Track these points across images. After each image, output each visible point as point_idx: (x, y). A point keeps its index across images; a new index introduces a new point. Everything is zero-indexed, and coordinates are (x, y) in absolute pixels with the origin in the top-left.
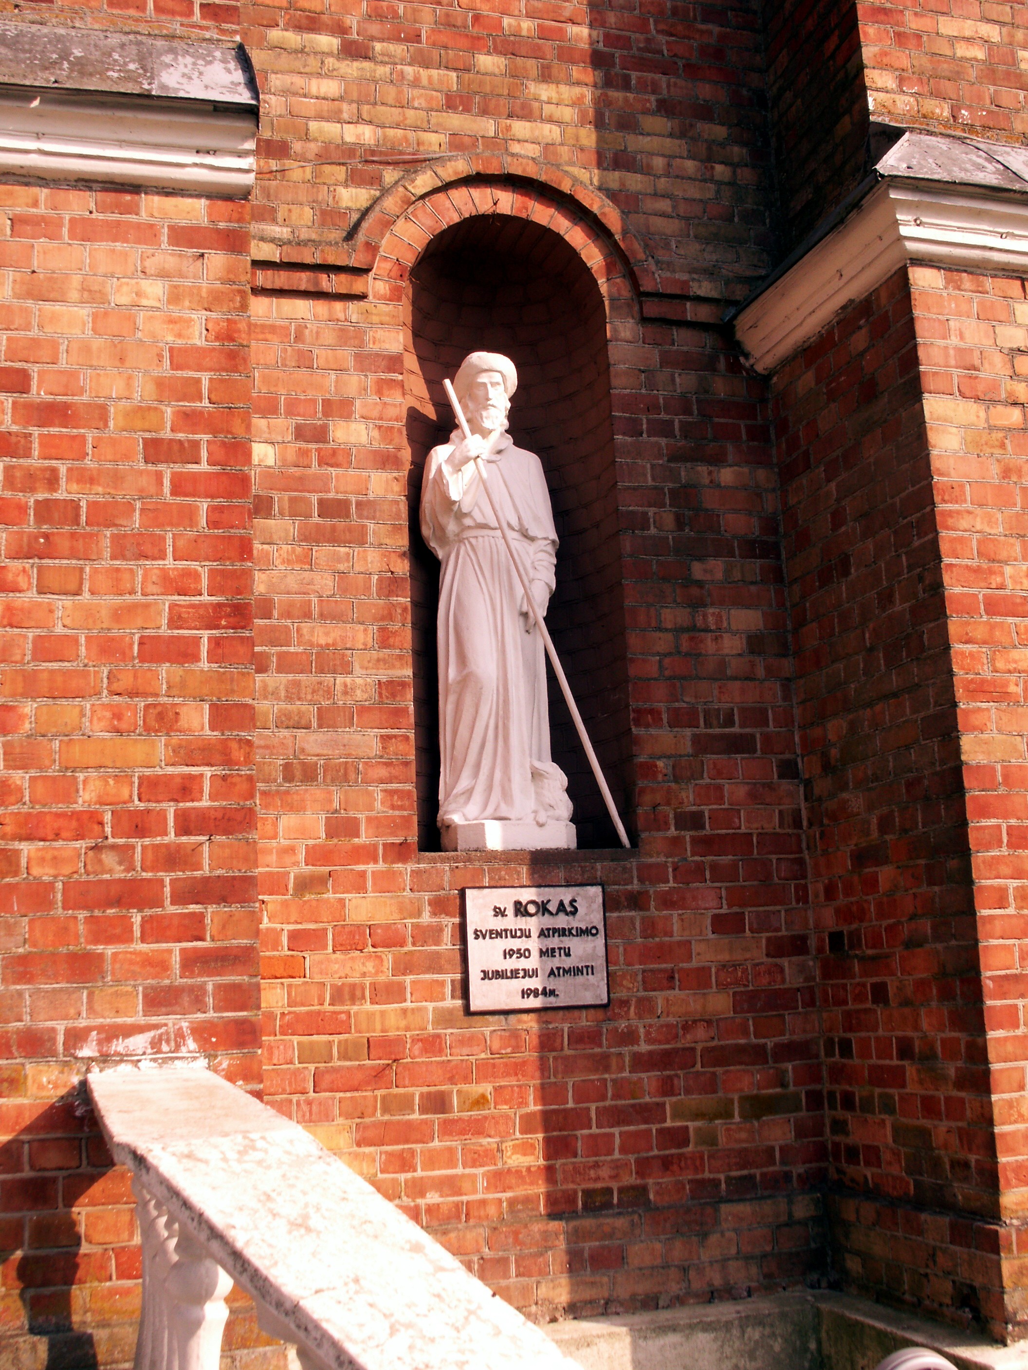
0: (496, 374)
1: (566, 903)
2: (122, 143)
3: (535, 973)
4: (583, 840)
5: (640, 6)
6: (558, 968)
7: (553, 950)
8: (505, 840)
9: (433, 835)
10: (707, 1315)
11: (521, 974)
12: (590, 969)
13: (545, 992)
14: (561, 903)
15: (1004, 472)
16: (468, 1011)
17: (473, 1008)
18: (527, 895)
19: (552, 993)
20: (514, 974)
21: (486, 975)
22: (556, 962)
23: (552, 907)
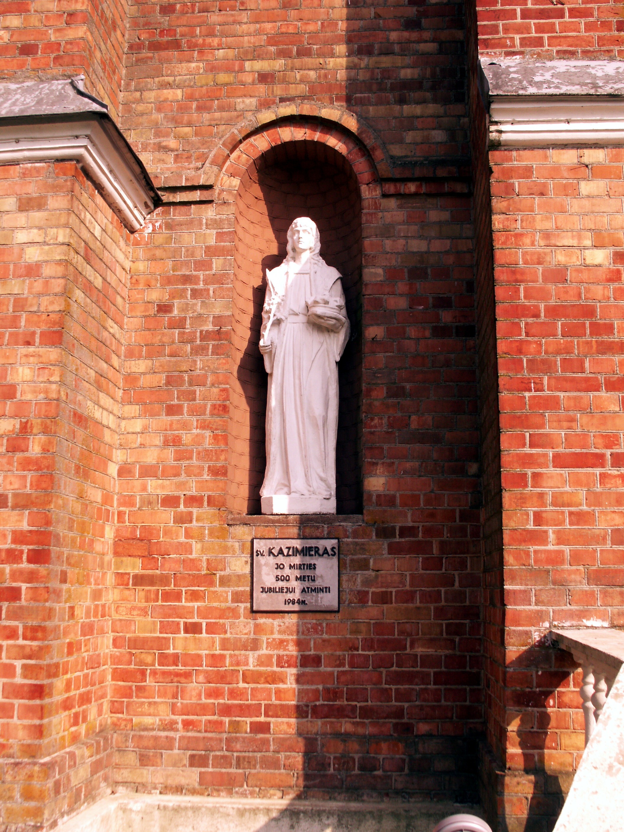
0: (306, 231)
1: (329, 549)
2: (34, 139)
3: (293, 591)
4: (341, 508)
5: (257, 22)
6: (308, 588)
7: (304, 577)
8: (289, 510)
9: (255, 506)
10: (169, 801)
11: (285, 590)
12: (327, 590)
13: (299, 602)
14: (281, 549)
15: (165, 306)
16: (338, 611)
17: (255, 608)
18: (297, 544)
19: (303, 602)
20: (281, 590)
21: (263, 590)
22: (306, 584)
23: (275, 552)
